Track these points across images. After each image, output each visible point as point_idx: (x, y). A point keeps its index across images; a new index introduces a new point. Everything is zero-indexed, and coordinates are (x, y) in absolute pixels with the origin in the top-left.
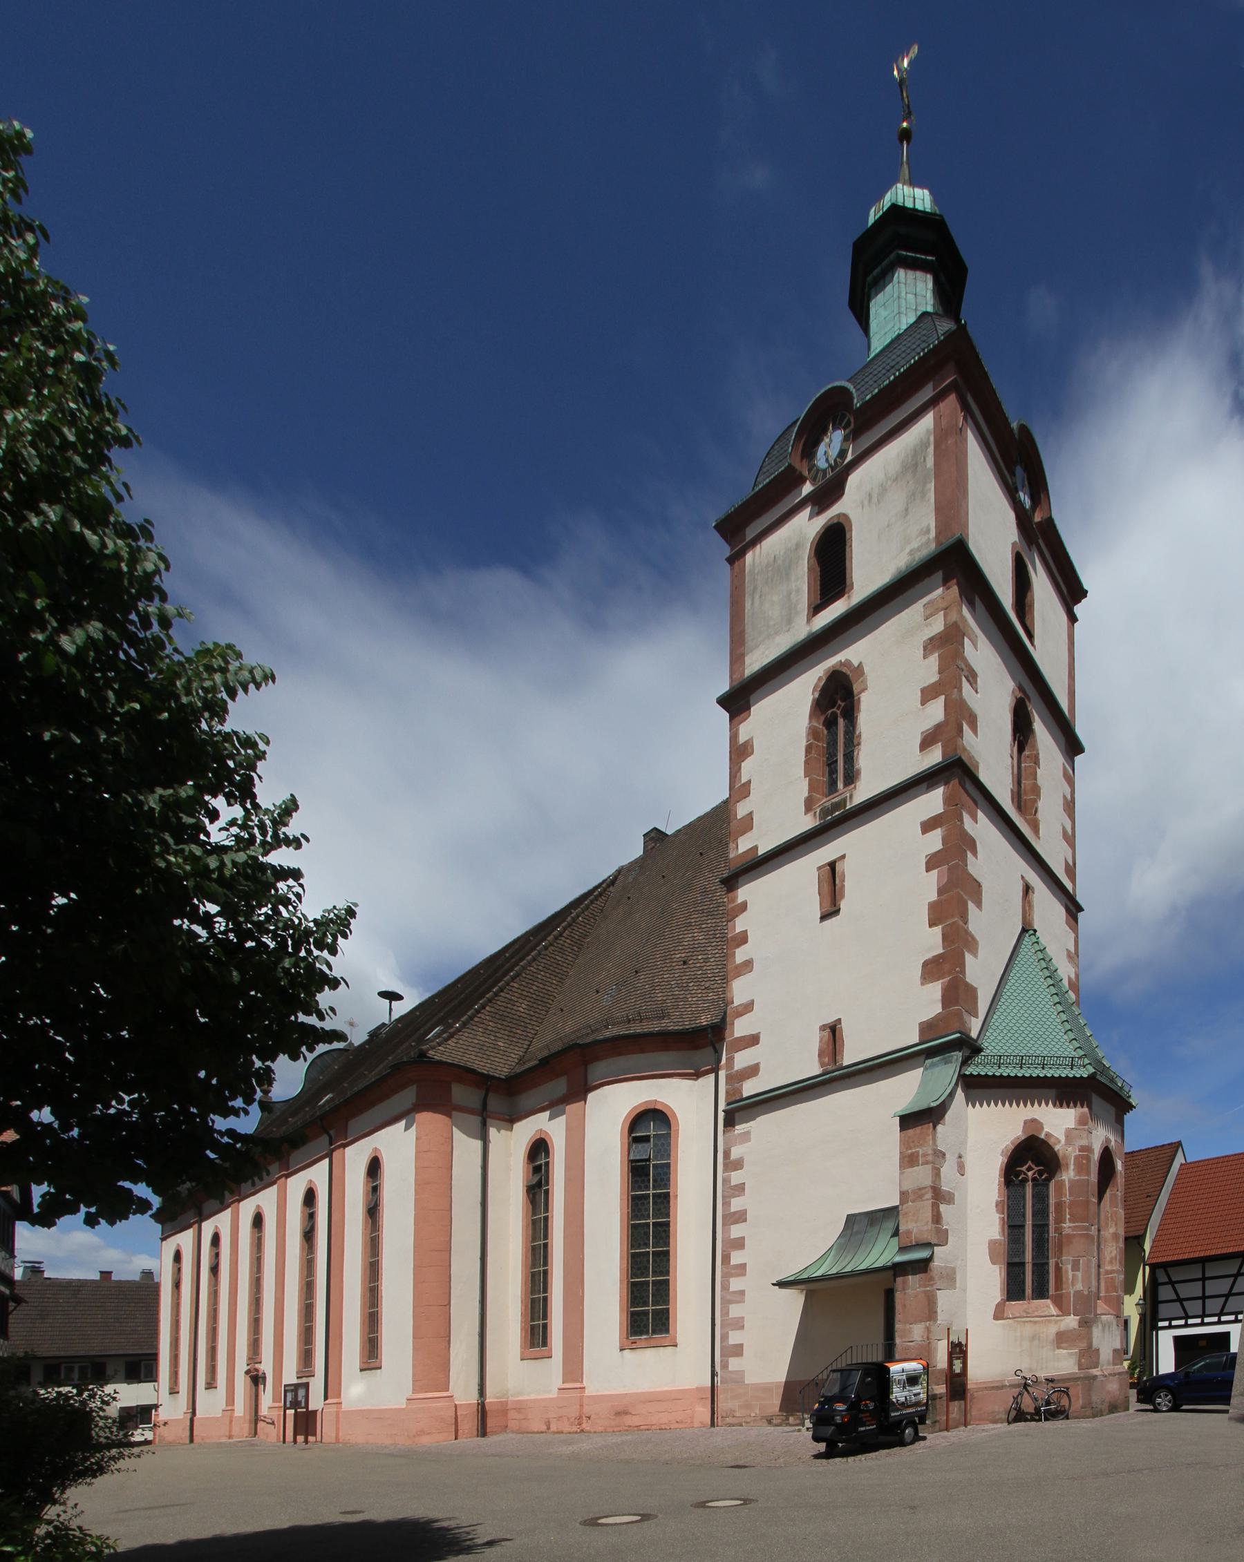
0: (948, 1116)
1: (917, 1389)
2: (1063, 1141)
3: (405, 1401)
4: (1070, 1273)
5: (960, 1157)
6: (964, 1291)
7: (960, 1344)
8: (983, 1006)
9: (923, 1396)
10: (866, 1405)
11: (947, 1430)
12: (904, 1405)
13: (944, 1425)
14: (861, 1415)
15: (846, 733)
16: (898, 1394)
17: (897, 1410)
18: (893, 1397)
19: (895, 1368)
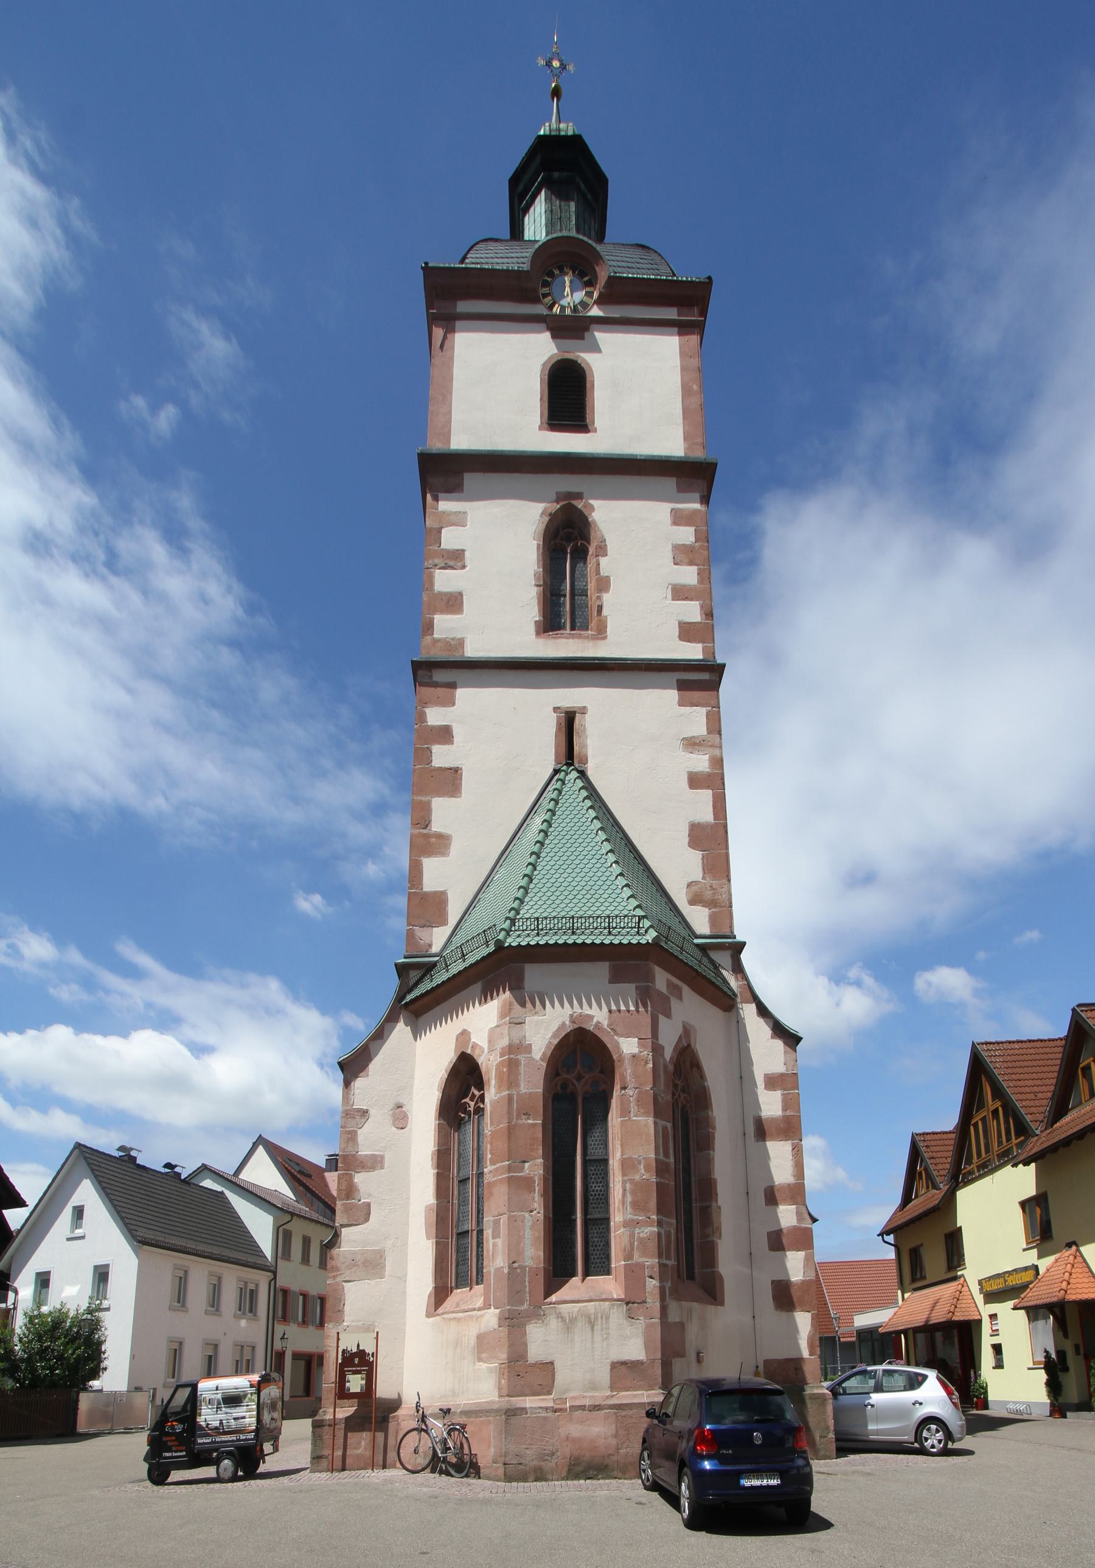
0: (373, 1066)
1: (238, 1412)
2: (486, 1051)
3: (604, 1376)
4: (491, 1241)
5: (400, 1107)
6: (403, 1278)
7: (361, 1354)
8: (453, 918)
9: (251, 1421)
10: (172, 1427)
11: (384, 1467)
12: (219, 1430)
13: (338, 1463)
14: (164, 1439)
15: (700, 681)
16: (208, 1416)
17: (207, 1435)
18: (201, 1420)
19: (206, 1386)
